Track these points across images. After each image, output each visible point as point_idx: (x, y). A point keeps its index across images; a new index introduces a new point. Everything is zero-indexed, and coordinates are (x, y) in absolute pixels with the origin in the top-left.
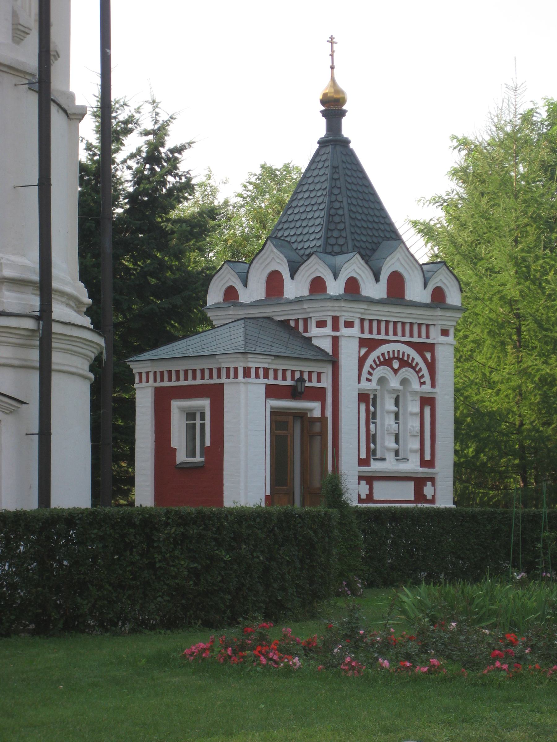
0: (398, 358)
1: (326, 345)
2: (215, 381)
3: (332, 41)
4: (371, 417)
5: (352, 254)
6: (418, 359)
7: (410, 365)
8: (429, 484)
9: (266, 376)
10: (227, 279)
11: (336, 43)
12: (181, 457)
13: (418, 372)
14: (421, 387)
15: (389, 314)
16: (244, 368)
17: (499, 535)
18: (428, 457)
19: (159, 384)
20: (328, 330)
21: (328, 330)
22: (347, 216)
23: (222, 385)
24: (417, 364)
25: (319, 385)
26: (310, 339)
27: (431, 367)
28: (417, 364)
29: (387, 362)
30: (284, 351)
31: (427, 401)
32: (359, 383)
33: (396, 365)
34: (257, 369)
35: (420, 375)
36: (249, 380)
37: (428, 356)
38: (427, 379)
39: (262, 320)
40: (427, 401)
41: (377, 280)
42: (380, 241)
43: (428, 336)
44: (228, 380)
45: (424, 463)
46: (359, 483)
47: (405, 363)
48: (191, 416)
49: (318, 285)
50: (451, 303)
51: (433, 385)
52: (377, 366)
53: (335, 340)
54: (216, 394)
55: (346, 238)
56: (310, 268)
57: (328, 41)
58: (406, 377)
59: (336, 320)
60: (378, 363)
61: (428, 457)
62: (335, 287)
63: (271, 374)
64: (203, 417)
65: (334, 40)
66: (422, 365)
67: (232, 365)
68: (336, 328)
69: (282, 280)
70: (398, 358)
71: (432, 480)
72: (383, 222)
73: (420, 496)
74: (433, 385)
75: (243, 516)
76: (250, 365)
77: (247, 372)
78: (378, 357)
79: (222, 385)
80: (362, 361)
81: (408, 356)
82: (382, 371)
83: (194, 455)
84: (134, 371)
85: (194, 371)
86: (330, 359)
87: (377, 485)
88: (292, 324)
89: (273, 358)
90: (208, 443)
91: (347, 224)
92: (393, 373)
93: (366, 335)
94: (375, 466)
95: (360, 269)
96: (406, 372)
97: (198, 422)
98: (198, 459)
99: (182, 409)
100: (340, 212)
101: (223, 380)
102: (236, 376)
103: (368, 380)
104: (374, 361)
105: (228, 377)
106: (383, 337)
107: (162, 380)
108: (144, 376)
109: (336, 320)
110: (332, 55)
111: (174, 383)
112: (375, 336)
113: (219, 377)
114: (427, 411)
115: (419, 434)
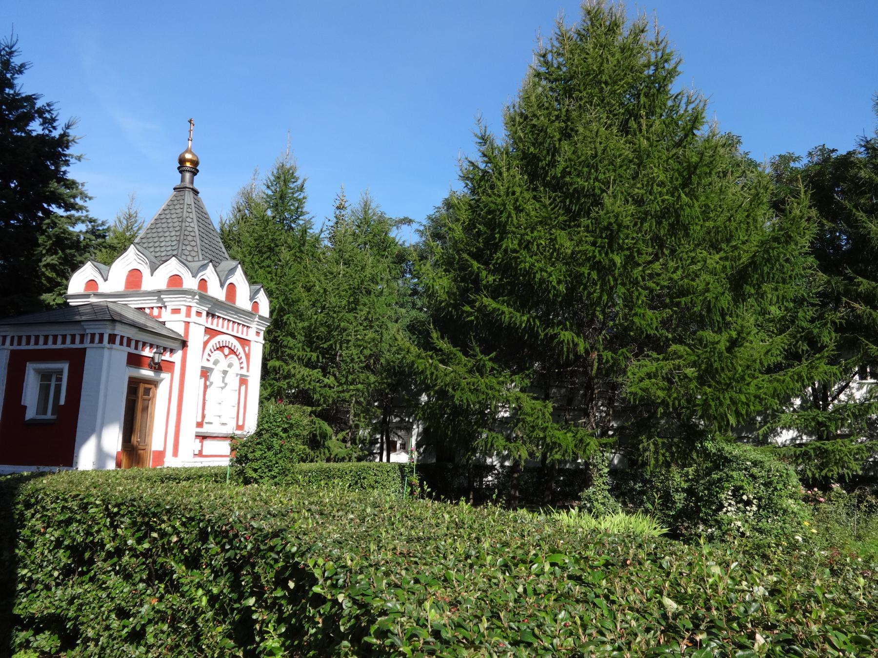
1: (180, 329)
2: (77, 345)
4: (206, 387)
9: (129, 345)
12: (31, 413)
16: (110, 335)
17: (322, 483)
18: (240, 423)
19: (15, 347)
20: (182, 316)
21: (182, 316)
22: (198, 237)
23: (84, 350)
26: (164, 323)
27: (248, 356)
29: (221, 348)
31: (243, 381)
33: (226, 351)
34: (122, 337)
36: (114, 346)
37: (247, 349)
38: (245, 365)
40: (243, 381)
41: (222, 285)
44: (91, 345)
47: (232, 351)
48: (45, 376)
49: (175, 280)
51: (248, 371)
54: (77, 360)
63: (133, 344)
64: (59, 379)
66: (242, 355)
68: (188, 315)
69: (141, 276)
74: (248, 371)
76: (116, 333)
77: (112, 339)
79: (85, 349)
80: (206, 344)
82: (218, 355)
83: (45, 413)
84: (111, 176)
87: (207, 443)
90: (62, 402)
94: (206, 429)
97: (53, 384)
98: (49, 416)
99: (38, 371)
100: (192, 234)
101: (87, 344)
103: (208, 360)
105: (92, 341)
106: (219, 329)
107: (19, 344)
113: (82, 342)
114: (243, 388)
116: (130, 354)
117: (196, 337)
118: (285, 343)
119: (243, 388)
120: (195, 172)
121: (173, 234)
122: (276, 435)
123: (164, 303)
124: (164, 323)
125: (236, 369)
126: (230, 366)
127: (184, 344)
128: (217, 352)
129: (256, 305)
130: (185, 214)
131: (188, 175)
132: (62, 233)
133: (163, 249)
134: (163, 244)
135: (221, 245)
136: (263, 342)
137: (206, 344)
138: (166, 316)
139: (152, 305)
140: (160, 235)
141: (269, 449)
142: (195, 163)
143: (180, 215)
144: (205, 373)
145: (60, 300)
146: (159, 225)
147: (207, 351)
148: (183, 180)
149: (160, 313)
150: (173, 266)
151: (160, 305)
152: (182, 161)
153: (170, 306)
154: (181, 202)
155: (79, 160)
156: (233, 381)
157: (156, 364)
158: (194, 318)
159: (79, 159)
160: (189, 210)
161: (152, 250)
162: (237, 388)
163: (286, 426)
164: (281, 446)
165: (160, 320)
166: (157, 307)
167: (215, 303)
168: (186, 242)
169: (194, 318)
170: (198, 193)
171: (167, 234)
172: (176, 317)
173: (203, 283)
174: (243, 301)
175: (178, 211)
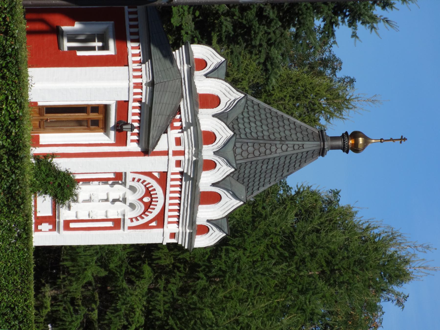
0: (152, 201)
1: (161, 146)
3: (402, 139)
4: (105, 181)
5: (234, 165)
6: (151, 216)
7: (146, 210)
8: (51, 227)
10: (213, 61)
11: (401, 142)
13: (140, 216)
14: (129, 219)
15: (187, 193)
18: (72, 225)
20: (173, 147)
21: (173, 147)
22: (265, 157)
24: (147, 216)
25: (128, 141)
26: (166, 132)
27: (145, 226)
28: (147, 216)
29: (148, 193)
30: (156, 114)
31: (117, 224)
32: (131, 172)
33: (146, 200)
35: (138, 218)
37: (154, 224)
39: (180, 92)
40: (117, 224)
41: (214, 185)
42: (245, 184)
43: (169, 223)
44: (131, 70)
45: (67, 224)
46: (41, 230)
47: (148, 206)
49: (210, 138)
50: (196, 240)
51: (130, 228)
52: (145, 186)
53: (166, 153)
55: (248, 158)
56: (223, 131)
57: (402, 136)
58: (136, 209)
59: (182, 153)
60: (147, 186)
61: (72, 225)
62: (208, 152)
64: (101, 49)
65: (403, 141)
67: (144, 73)
68: (176, 153)
70: (152, 201)
71: (54, 229)
72: (260, 184)
73: (41, 220)
74: (130, 228)
75: (20, 84)
78: (152, 186)
79: (128, 65)
80: (149, 174)
81: (154, 209)
82: (141, 190)
85: (136, 20)
86: (150, 149)
88: (178, 117)
89: (150, 106)
91: (259, 158)
92: (139, 198)
93: (170, 177)
95: (223, 171)
96: (140, 208)
100: (268, 152)
102: (135, 77)
103: (134, 179)
104: (149, 183)
105: (135, 70)
106: (169, 189)
108: (139, 74)
109: (182, 153)
110: (391, 139)
111: (127, 23)
112: (169, 183)
114: (110, 224)
115: (90, 219)
116: (127, 102)
117: (154, 164)
118: (172, 280)
119: (110, 224)
120: (345, 149)
121: (266, 133)
122: (56, 179)
123: (186, 129)
124: (166, 132)
125: (130, 214)
126: (132, 206)
127: (146, 152)
128: (144, 190)
129: (203, 230)
130: (291, 143)
131: (340, 143)
132: (255, 31)
133: (247, 125)
134: (253, 125)
135: (267, 186)
136: (165, 243)
137: (149, 174)
138: (173, 134)
139: (183, 120)
140: (264, 122)
141: (47, 176)
142: (356, 149)
143: (289, 138)
144: (119, 178)
145: (185, 38)
146: (275, 119)
147: (143, 177)
148: (334, 138)
149: (176, 128)
150: (223, 133)
151: (184, 125)
152: (355, 135)
153: (184, 136)
154: (305, 139)
155: (353, 36)
156: (114, 212)
157: (121, 127)
158: (173, 159)
159: (354, 35)
160: (296, 147)
161: (246, 115)
162: (110, 217)
163: (62, 185)
164: (49, 183)
165: (169, 129)
166: (182, 125)
167: (195, 181)
168: (256, 146)
169: (173, 159)
170: (323, 155)
171: (265, 127)
172: (173, 142)
173: (210, 165)
174: (206, 213)
175: (294, 136)
